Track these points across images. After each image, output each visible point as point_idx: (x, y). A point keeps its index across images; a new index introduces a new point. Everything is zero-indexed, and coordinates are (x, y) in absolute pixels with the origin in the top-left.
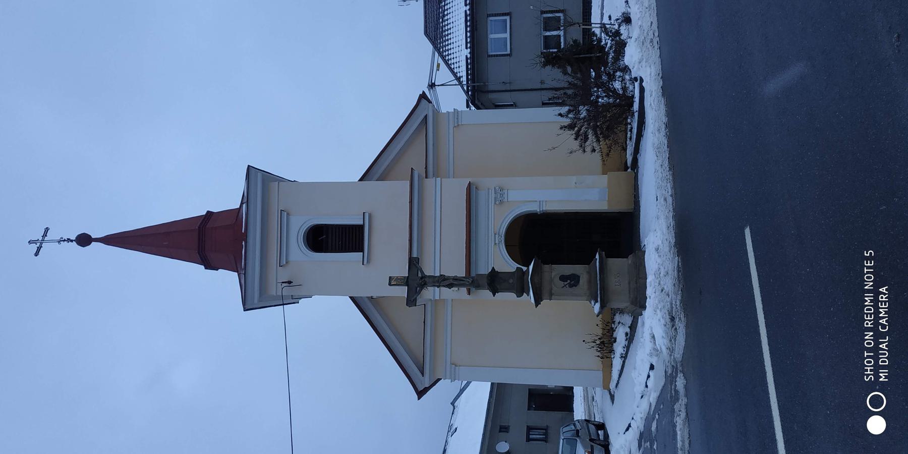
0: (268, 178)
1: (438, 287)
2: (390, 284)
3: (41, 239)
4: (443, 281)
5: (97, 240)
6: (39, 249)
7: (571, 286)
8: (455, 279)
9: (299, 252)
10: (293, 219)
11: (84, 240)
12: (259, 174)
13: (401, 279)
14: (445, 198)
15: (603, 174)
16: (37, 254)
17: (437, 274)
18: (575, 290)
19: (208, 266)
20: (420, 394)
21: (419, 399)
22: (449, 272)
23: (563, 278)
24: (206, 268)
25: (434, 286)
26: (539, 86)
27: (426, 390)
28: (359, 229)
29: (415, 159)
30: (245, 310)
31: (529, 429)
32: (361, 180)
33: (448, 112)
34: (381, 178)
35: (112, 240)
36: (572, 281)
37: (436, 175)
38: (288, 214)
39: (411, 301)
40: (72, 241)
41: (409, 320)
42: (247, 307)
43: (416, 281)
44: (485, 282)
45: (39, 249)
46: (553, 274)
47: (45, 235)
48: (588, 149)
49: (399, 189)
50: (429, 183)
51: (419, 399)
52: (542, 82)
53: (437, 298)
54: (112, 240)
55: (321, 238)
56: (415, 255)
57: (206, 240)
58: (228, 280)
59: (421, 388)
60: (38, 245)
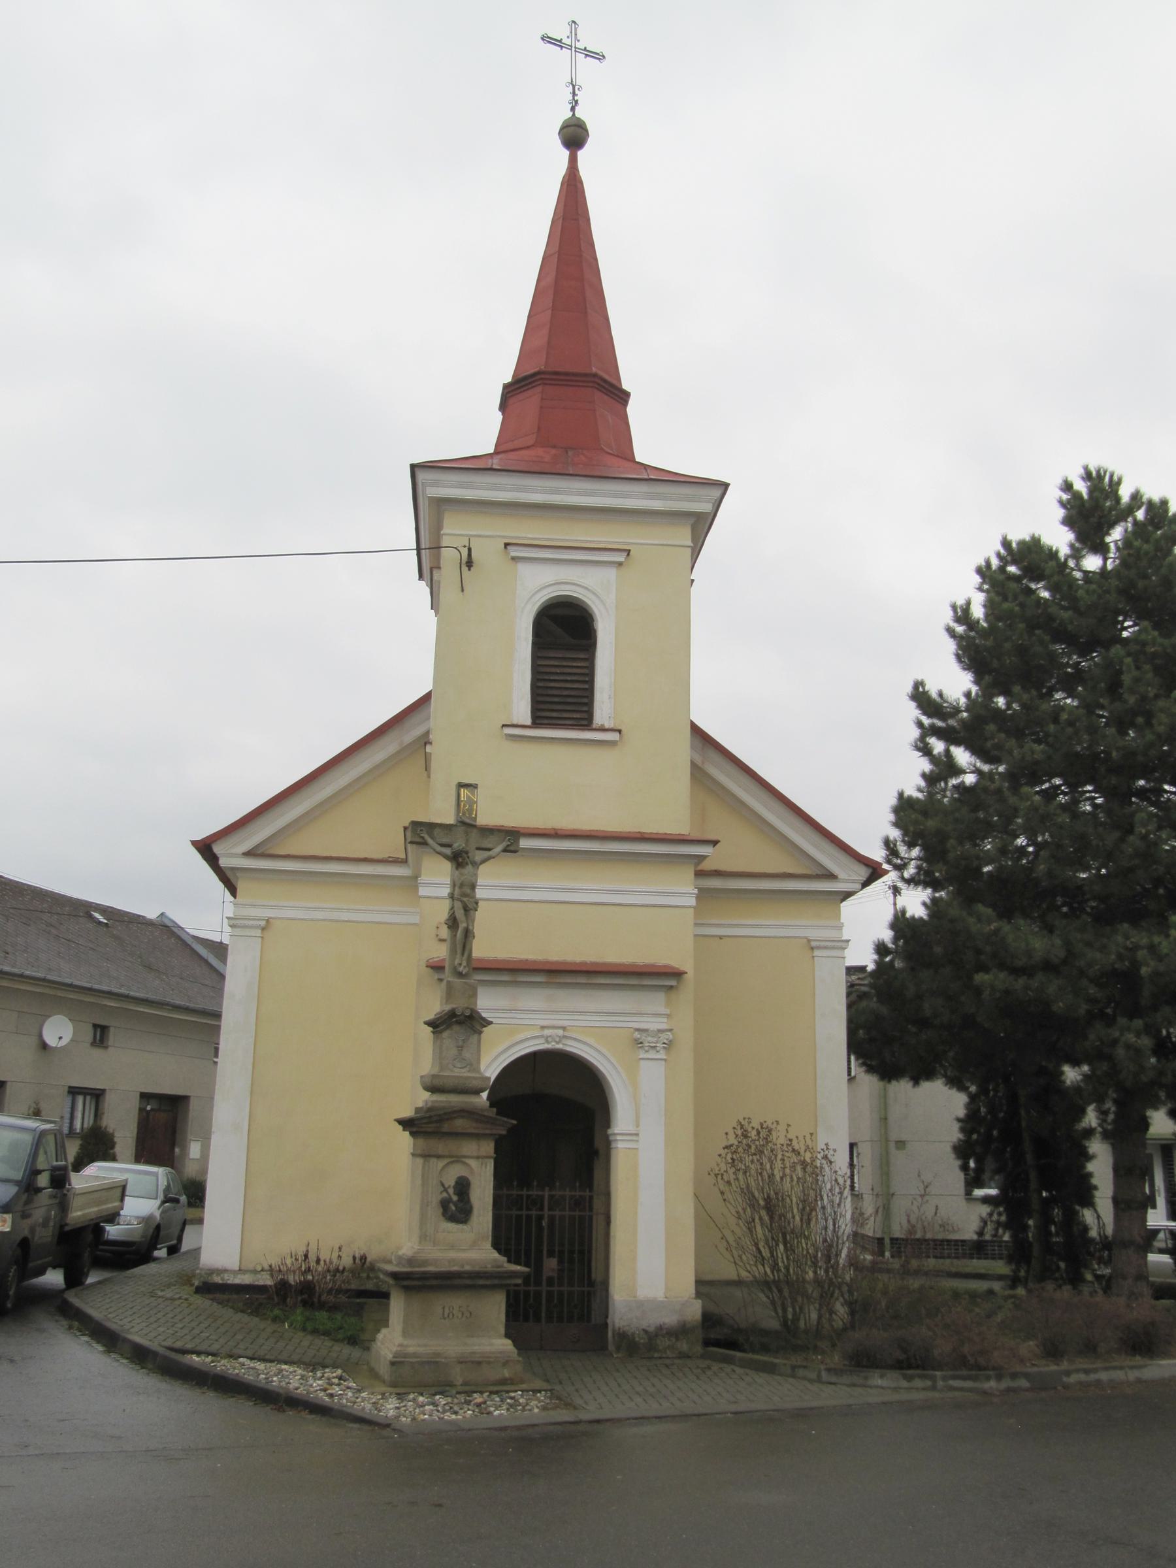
0: (700, 525)
1: (452, 896)
2: (461, 786)
3: (580, 45)
4: (464, 902)
5: (573, 161)
6: (558, 43)
7: (445, 1204)
8: (468, 934)
9: (538, 584)
10: (612, 573)
11: (574, 136)
12: (707, 508)
13: (470, 810)
14: (648, 914)
15: (699, 1283)
16: (546, 39)
17: (480, 893)
18: (435, 1212)
19: (511, 393)
20: (206, 848)
21: (194, 843)
22: (482, 921)
23: (463, 1187)
24: (506, 387)
25: (454, 885)
26: (894, 1136)
27: (211, 858)
28: (585, 720)
29: (740, 850)
30: (413, 467)
31: (97, 1096)
32: (696, 730)
33: (840, 927)
34: (698, 773)
35: (572, 192)
36: (457, 1207)
37: (703, 895)
38: (620, 564)
39: (421, 834)
40: (573, 109)
41: (374, 827)
42: (421, 476)
43: (464, 843)
44: (460, 1004)
45: (558, 43)
46: (473, 1163)
47: (588, 53)
48: (801, 1138)
49: (669, 808)
50: (689, 873)
51: (194, 843)
52: (901, 1144)
53: (422, 891)
54: (572, 192)
55: (565, 631)
56: (524, 843)
57: (566, 390)
58: (480, 431)
59: (217, 849)
60: (566, 41)
